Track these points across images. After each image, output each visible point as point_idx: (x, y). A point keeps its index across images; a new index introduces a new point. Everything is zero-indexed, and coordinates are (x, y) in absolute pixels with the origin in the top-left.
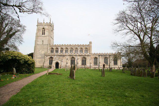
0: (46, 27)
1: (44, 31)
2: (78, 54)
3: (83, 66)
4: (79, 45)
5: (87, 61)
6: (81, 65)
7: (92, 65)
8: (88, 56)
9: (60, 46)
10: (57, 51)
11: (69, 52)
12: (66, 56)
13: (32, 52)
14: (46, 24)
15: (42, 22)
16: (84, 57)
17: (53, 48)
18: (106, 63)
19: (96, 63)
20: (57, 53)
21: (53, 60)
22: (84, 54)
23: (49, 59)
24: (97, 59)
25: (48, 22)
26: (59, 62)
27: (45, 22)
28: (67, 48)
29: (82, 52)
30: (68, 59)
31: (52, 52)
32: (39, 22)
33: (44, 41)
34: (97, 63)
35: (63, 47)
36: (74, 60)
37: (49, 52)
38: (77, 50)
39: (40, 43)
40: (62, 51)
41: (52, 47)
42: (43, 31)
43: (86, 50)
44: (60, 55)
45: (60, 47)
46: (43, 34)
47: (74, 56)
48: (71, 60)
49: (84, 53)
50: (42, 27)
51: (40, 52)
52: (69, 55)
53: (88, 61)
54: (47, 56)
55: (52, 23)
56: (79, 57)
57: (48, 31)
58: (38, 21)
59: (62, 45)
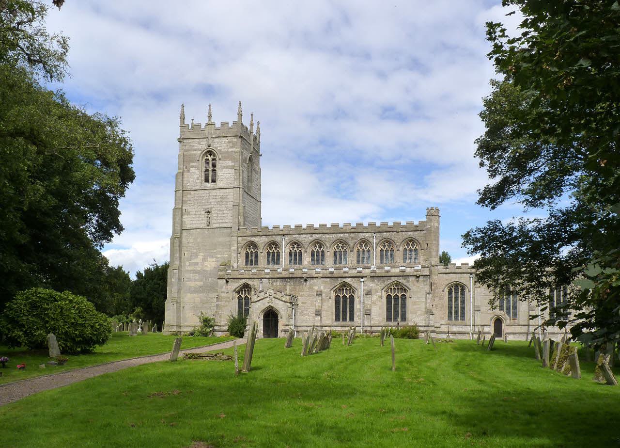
0: (221, 146)
1: (214, 164)
2: (367, 272)
3: (390, 323)
4: (316, 226)
5: (409, 302)
6: (385, 322)
7: (440, 319)
8: (418, 277)
9: (287, 232)
10: (274, 258)
11: (329, 259)
12: (315, 281)
13: (160, 264)
14: (218, 129)
15: (203, 121)
16: (397, 284)
17: (253, 245)
18: (508, 313)
19: (456, 312)
20: (276, 267)
21: (254, 298)
22: (397, 270)
23: (336, 291)
24: (463, 290)
25: (231, 119)
26: (281, 307)
27: (213, 120)
28: (318, 243)
29: (393, 260)
30: (321, 292)
31: (251, 259)
32: (188, 121)
33: (213, 215)
34: (463, 313)
35: (302, 238)
36: (352, 297)
37: (238, 261)
38: (369, 251)
39: (194, 219)
40: (295, 257)
41: (253, 239)
42: (207, 165)
43: (411, 250)
44: (285, 274)
45: (287, 238)
46: (207, 180)
47: (348, 280)
48: (337, 297)
49: (398, 266)
50: (203, 145)
51: (197, 264)
52: (326, 273)
53: (415, 303)
54: (227, 282)
55: (252, 125)
56: (372, 285)
57: (230, 163)
58: (183, 118)
59: (298, 227)
